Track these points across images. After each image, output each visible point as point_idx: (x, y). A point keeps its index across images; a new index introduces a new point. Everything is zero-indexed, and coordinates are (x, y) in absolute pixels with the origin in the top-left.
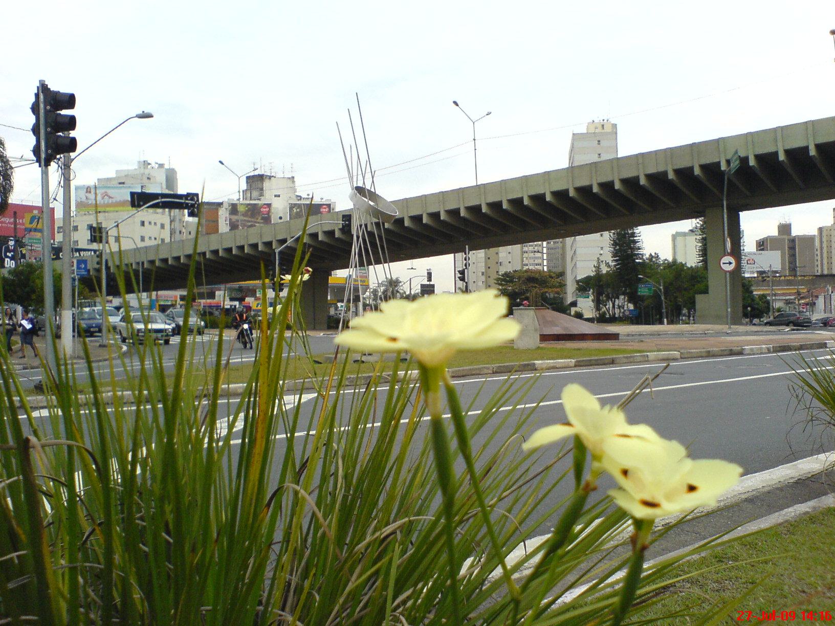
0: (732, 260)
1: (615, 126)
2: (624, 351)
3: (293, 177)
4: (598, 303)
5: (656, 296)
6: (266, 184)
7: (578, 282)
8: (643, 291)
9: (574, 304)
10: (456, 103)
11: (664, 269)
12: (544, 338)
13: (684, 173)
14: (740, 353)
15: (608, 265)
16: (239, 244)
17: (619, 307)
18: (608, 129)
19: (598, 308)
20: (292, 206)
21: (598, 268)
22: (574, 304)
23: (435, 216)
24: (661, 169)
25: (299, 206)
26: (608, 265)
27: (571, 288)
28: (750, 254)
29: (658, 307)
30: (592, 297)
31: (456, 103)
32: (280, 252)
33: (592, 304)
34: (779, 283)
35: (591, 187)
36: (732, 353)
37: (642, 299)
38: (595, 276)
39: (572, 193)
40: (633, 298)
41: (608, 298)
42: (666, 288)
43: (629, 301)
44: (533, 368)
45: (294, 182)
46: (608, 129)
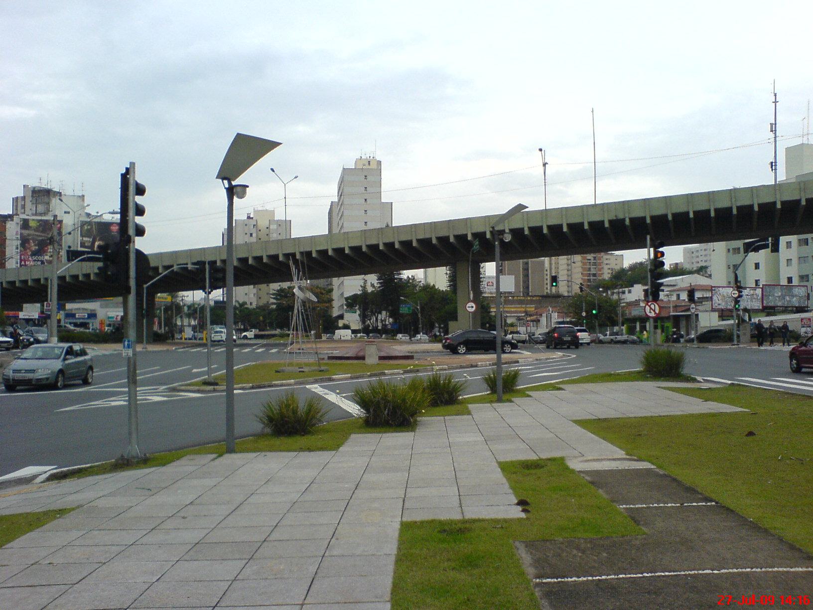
0: (474, 305)
1: (379, 163)
2: (422, 366)
3: (83, 196)
4: (364, 317)
5: (414, 314)
6: (55, 201)
7: (347, 299)
8: (404, 310)
9: (341, 317)
10: (272, 170)
11: (420, 291)
12: (381, 358)
13: (443, 240)
14: (476, 366)
15: (373, 285)
16: (84, 272)
17: (382, 321)
18: (373, 166)
19: (363, 322)
20: (83, 224)
21: (364, 287)
22: (341, 317)
23: (259, 259)
24: (428, 236)
25: (90, 223)
26: (373, 285)
27: (336, 304)
28: (489, 277)
29: (415, 322)
30: (358, 312)
31: (272, 170)
32: (147, 288)
33: (358, 318)
34: (512, 302)
35: (378, 245)
36: (472, 366)
37: (402, 315)
38: (361, 295)
39: (364, 249)
40: (394, 314)
41: (373, 313)
42: (422, 308)
43: (390, 317)
44: (384, 374)
45: (83, 200)
46: (373, 166)
